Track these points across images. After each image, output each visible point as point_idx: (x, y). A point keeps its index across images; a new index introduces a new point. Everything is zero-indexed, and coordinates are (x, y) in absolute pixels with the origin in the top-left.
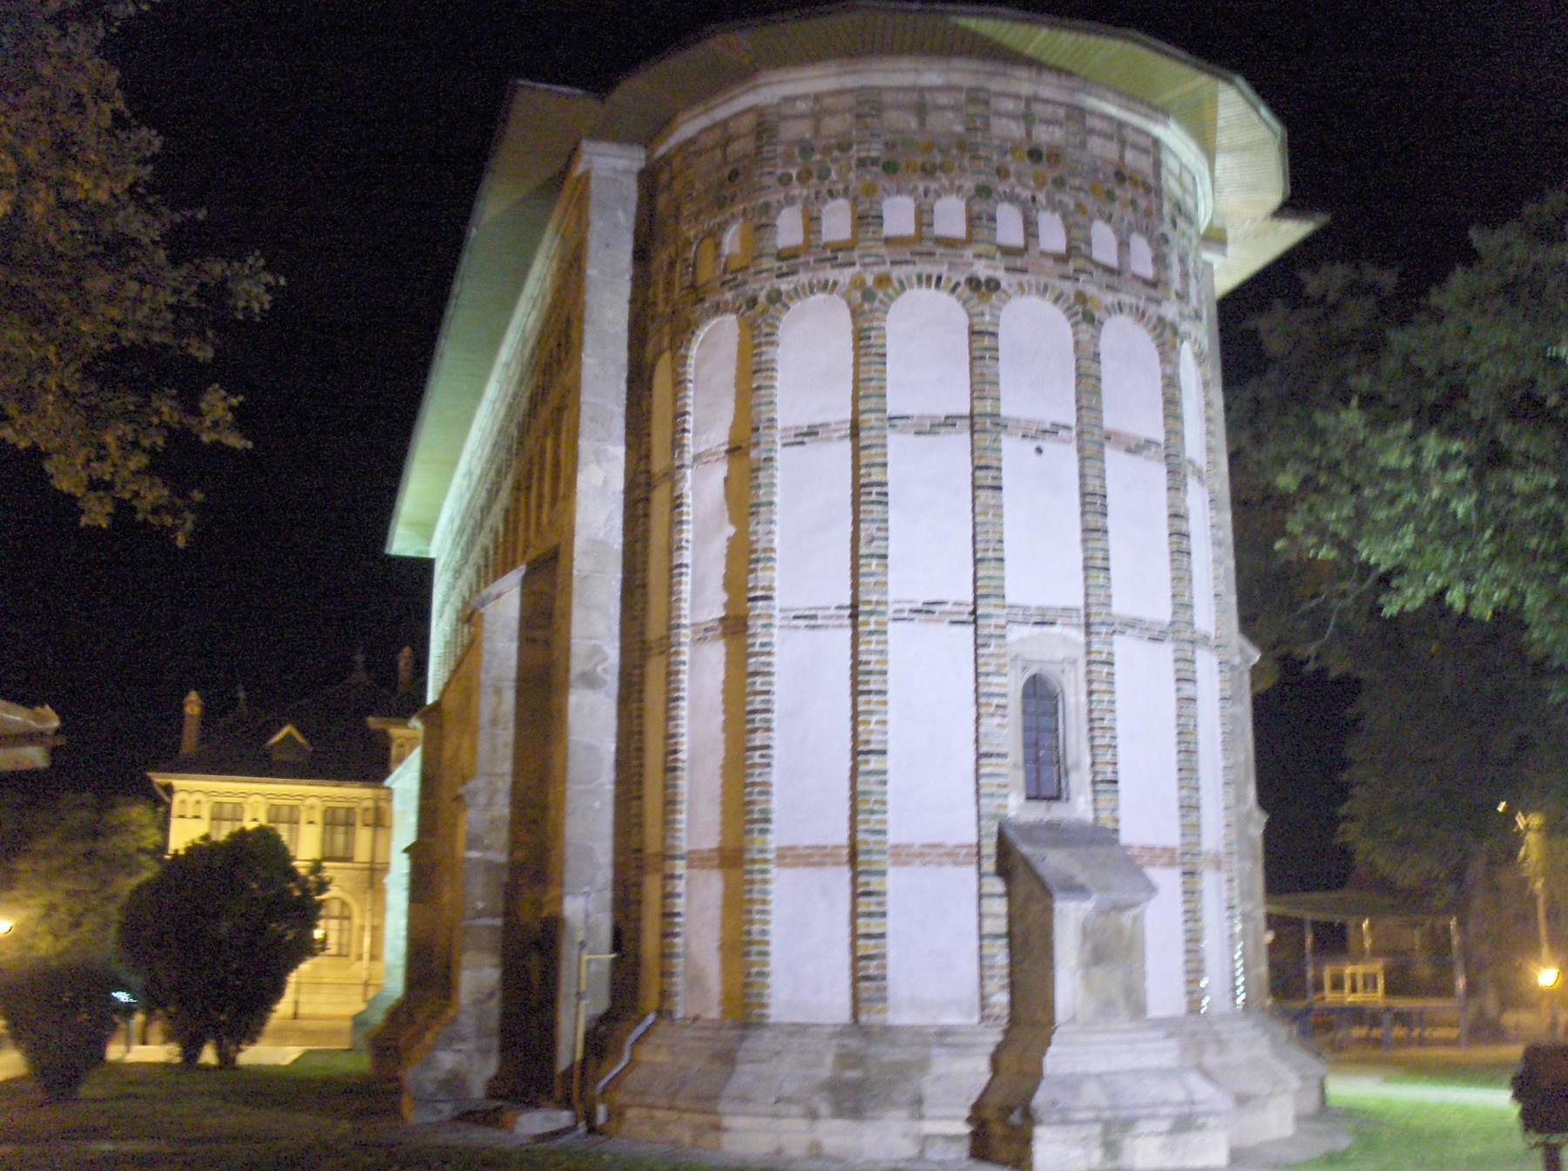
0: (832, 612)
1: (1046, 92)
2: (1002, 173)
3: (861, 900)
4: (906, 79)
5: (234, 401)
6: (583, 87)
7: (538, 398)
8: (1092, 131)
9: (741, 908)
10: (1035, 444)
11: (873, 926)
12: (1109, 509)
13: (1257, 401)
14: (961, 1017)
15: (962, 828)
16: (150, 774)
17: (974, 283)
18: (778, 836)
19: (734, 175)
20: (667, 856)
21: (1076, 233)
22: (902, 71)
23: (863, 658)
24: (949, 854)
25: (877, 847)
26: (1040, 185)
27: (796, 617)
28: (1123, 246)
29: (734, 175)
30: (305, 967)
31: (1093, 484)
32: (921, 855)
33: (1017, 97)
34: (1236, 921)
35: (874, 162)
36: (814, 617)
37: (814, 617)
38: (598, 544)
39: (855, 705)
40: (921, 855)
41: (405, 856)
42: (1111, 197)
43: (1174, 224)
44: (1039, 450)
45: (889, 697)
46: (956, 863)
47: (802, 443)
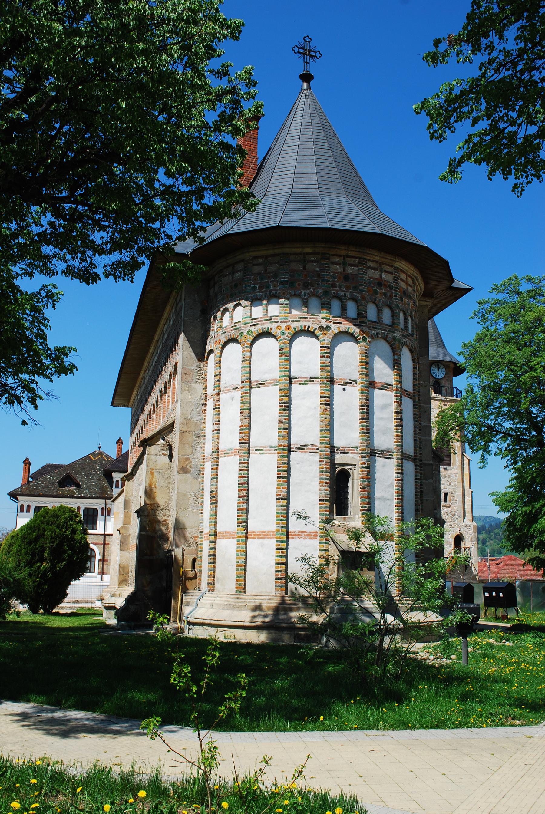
0: (269, 448)
1: (351, 254)
2: (333, 286)
3: (213, 540)
4: (299, 251)
5: (41, 611)
6: (177, 724)
7: (419, 493)
8: (370, 268)
9: (90, 577)
10: (343, 387)
11: (243, 480)
12: (217, 561)
13: (250, 187)
14: (358, 445)
15: (45, 310)
16: (182, 338)
17: (321, 328)
18: (272, 543)
19: (236, 286)
20: (404, 457)
21: (361, 308)
22: (297, 247)
23: (285, 512)
24: (308, 535)
25: (202, 784)
26: (348, 288)
27: (256, 450)
28: (380, 311)
29: (236, 286)
30: (87, 574)
31: (286, 413)
32: (298, 535)
33: (340, 256)
34: (199, 208)
35: (286, 282)
36: (262, 450)
37: (262, 450)
38: (385, 432)
39: (246, 548)
40: (298, 535)
41: (460, 281)
42: (376, 292)
43: (402, 300)
44: (344, 390)
45: (276, 497)
46: (310, 539)
47: (387, 384)
